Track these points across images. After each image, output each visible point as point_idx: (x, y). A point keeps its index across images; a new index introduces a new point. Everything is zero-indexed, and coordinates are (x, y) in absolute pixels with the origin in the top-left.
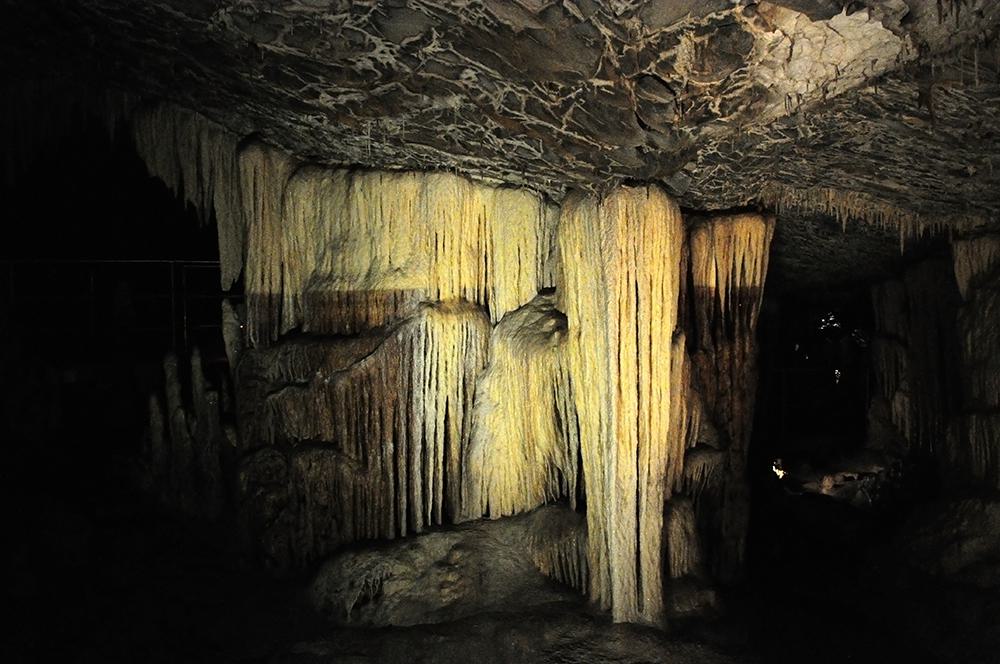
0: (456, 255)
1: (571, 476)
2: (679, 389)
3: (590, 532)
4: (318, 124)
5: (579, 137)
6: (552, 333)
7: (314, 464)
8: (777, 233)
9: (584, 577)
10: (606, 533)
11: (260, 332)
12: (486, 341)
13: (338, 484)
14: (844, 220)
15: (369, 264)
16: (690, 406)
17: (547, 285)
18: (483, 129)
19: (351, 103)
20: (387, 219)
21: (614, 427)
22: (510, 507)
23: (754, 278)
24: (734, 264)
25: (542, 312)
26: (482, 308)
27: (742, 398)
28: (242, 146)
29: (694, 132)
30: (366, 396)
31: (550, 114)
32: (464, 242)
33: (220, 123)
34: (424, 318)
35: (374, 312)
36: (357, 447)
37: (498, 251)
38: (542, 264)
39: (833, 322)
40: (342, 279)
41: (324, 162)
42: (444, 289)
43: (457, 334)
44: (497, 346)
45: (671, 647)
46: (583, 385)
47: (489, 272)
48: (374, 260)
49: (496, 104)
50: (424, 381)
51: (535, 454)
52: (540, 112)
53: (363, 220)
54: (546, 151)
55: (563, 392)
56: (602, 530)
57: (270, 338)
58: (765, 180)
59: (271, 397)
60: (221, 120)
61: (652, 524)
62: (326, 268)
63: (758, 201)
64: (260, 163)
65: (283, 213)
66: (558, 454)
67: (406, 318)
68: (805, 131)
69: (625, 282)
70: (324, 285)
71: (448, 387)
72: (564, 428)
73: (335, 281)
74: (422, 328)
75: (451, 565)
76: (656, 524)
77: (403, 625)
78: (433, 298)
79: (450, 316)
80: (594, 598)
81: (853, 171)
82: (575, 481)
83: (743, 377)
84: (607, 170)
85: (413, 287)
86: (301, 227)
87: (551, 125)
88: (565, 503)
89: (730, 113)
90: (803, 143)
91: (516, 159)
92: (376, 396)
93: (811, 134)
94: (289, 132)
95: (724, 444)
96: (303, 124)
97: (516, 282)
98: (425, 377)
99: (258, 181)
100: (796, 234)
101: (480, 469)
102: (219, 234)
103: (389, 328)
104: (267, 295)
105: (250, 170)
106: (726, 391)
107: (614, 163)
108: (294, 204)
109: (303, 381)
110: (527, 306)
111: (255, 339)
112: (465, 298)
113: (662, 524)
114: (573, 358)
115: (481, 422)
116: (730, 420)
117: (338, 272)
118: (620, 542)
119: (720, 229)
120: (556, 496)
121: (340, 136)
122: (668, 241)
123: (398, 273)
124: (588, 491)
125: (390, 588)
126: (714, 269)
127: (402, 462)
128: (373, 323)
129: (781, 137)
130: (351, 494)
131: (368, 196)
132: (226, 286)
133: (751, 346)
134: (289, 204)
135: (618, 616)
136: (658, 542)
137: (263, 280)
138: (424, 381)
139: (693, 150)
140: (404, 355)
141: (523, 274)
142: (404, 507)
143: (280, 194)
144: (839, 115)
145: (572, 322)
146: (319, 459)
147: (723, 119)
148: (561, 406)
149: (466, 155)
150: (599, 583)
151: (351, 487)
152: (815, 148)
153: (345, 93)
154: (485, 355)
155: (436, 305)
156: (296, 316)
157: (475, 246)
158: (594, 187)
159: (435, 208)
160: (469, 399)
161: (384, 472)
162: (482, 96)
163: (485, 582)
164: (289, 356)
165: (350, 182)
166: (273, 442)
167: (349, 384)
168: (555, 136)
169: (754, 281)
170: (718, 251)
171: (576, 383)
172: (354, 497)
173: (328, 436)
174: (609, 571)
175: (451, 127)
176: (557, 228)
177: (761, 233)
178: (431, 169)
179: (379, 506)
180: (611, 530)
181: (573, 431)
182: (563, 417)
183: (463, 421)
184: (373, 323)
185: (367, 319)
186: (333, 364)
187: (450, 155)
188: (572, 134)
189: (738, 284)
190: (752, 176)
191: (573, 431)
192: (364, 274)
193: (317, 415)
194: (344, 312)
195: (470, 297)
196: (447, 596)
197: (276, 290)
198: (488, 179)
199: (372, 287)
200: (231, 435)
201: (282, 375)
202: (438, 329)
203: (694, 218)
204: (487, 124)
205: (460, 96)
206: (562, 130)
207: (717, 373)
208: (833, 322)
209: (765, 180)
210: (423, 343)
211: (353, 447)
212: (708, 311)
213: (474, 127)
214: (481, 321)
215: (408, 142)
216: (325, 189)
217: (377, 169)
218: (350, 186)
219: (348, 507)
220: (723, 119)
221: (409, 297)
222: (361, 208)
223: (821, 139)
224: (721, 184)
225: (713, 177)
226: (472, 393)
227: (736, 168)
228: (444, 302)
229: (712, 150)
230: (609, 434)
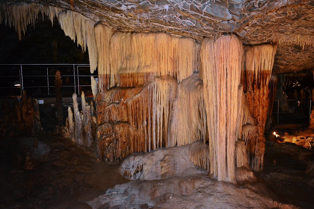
0: (166, 61)
1: (204, 132)
2: (241, 104)
3: (210, 151)
4: (121, 17)
5: (208, 18)
6: (198, 86)
7: (121, 128)
8: (277, 52)
9: (208, 166)
10: (215, 151)
11: (104, 86)
12: (176, 89)
13: (129, 134)
14: (303, 46)
15: (138, 64)
16: (244, 110)
17: (196, 70)
18: (176, 16)
19: (133, 8)
20: (144, 49)
21: (218, 116)
22: (184, 143)
23: (268, 67)
24: (261, 63)
25: (195, 79)
26: (175, 78)
27: (263, 108)
28: (95, 25)
29: (249, 15)
30: (138, 107)
31: (199, 10)
32: (169, 56)
33: (88, 18)
34: (156, 81)
35: (140, 79)
36: (135, 123)
37: (180, 59)
38: (195, 63)
39: (298, 84)
40: (130, 69)
41: (123, 30)
42: (163, 72)
43: (167, 87)
44: (180, 90)
45: (238, 190)
46: (208, 103)
47: (177, 66)
48: (140, 63)
49: (181, 7)
50: (156, 102)
51: (192, 125)
52: (195, 9)
53: (136, 49)
54: (197, 24)
55: (202, 105)
56: (214, 150)
57: (107, 88)
58: (274, 32)
59: (107, 107)
60: (88, 16)
61: (231, 148)
62: (124, 66)
63: (271, 40)
64: (102, 31)
65: (110, 48)
66: (200, 126)
67: (150, 82)
68: (290, 13)
69: (222, 68)
70: (124, 71)
71: (164, 104)
72: (202, 117)
73: (127, 70)
74: (156, 84)
75: (165, 161)
76: (232, 148)
77: (150, 179)
78: (159, 75)
79: (164, 81)
80: (211, 172)
81: (308, 27)
82: (205, 134)
83: (263, 101)
84: (217, 29)
85: (153, 71)
86: (116, 52)
87: (198, 14)
88: (203, 141)
89: (262, 6)
90: (289, 18)
91: (187, 26)
92: (141, 106)
93: (292, 14)
94: (111, 20)
95: (256, 124)
96: (116, 17)
97: (186, 69)
98: (156, 100)
99: (102, 37)
100: (284, 52)
101: (174, 130)
102: (89, 57)
103: (145, 85)
104: (105, 75)
105: (99, 35)
106: (257, 106)
107: (220, 27)
108: (113, 45)
109: (118, 102)
110: (190, 77)
111: (102, 89)
112: (169, 75)
113: (234, 149)
114: (205, 94)
115: (174, 115)
116: (258, 115)
117: (128, 67)
118: (220, 154)
119: (256, 50)
120: (199, 139)
121: (129, 21)
122: (238, 54)
123: (148, 67)
124: (210, 137)
125: (145, 168)
126: (254, 64)
127: (149, 128)
128: (140, 83)
129: (281, 16)
130: (133, 138)
131: (138, 42)
132: (92, 72)
133: (266, 90)
134: (112, 45)
135: (220, 179)
136: (233, 154)
137: (104, 70)
138: (156, 102)
139: (248, 21)
140: (150, 93)
141: (188, 67)
142: (150, 142)
143: (109, 41)
144: (303, 6)
145: (205, 81)
146: (123, 126)
147: (259, 9)
148: (201, 109)
149: (170, 26)
150: (213, 166)
151: (133, 136)
152: (293, 20)
153: (130, 5)
154: (176, 94)
155: (160, 77)
156: (115, 81)
157: (172, 58)
158: (213, 36)
159: (159, 45)
160: (171, 108)
161: (144, 131)
162: (176, 5)
163: (176, 166)
164: (113, 94)
165: (131, 37)
166: (108, 121)
167: (132, 103)
168: (200, 18)
169: (268, 68)
170: (255, 58)
171: (206, 102)
172: (134, 139)
173: (126, 119)
174: (217, 163)
175: (165, 16)
176: (199, 51)
177: (271, 51)
178: (158, 32)
179: (142, 141)
180: (217, 150)
181: (204, 118)
182: (201, 113)
183: (169, 115)
184: (140, 83)
185: (138, 82)
186: (127, 96)
187: (164, 26)
188: (206, 17)
189: (262, 69)
190: (269, 31)
191: (204, 118)
192: (137, 67)
193: (122, 112)
194: (130, 80)
195: (171, 74)
196: (164, 171)
197: (108, 73)
198: (177, 35)
199: (139, 72)
200: (94, 119)
201: (111, 100)
202: (160, 85)
203: (247, 46)
204: (177, 14)
205: (169, 5)
206: (203, 16)
207: (254, 99)
208: (298, 84)
209: (274, 32)
210: (156, 89)
211: (134, 123)
212: (251, 78)
213: (173, 16)
214: (174, 83)
215: (151, 22)
216: (123, 39)
217: (140, 32)
218: (131, 38)
219: (132, 142)
220: (259, 9)
221: (151, 75)
222: (135, 45)
223: (296, 16)
224: (257, 34)
225: (254, 32)
226: (172, 105)
227: (263, 28)
228: (162, 76)
229: (254, 21)
230: (216, 118)
